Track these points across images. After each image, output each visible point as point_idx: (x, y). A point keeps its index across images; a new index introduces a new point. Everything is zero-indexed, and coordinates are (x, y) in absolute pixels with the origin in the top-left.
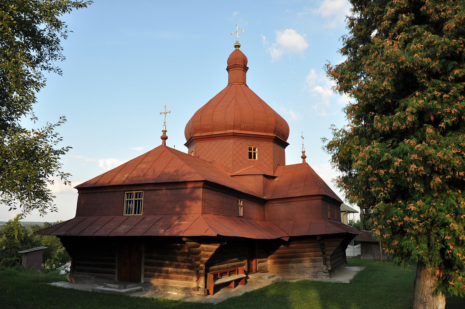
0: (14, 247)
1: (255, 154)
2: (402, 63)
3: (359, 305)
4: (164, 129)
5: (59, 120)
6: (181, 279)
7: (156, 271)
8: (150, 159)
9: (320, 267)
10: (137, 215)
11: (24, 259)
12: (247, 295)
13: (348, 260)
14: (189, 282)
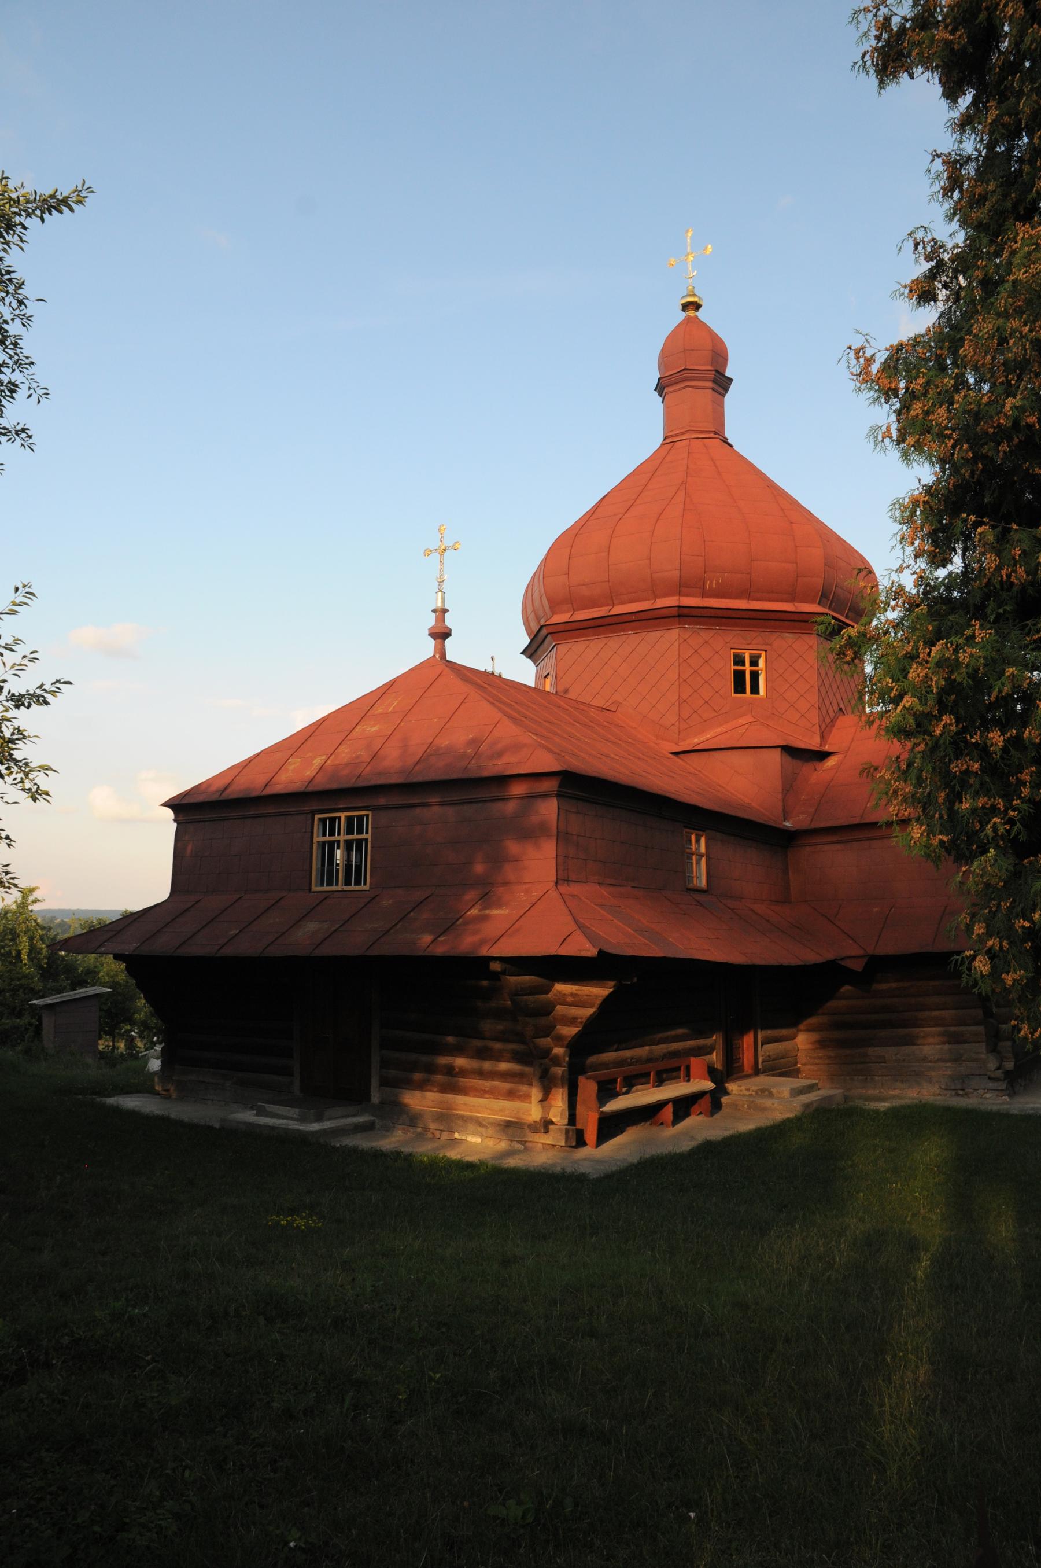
0: (21, 986)
1: (755, 676)
4: (439, 605)
5: (12, 596)
6: (494, 1093)
9: (976, 1060)
10: (353, 887)
11: (48, 1022)
12: (708, 1148)
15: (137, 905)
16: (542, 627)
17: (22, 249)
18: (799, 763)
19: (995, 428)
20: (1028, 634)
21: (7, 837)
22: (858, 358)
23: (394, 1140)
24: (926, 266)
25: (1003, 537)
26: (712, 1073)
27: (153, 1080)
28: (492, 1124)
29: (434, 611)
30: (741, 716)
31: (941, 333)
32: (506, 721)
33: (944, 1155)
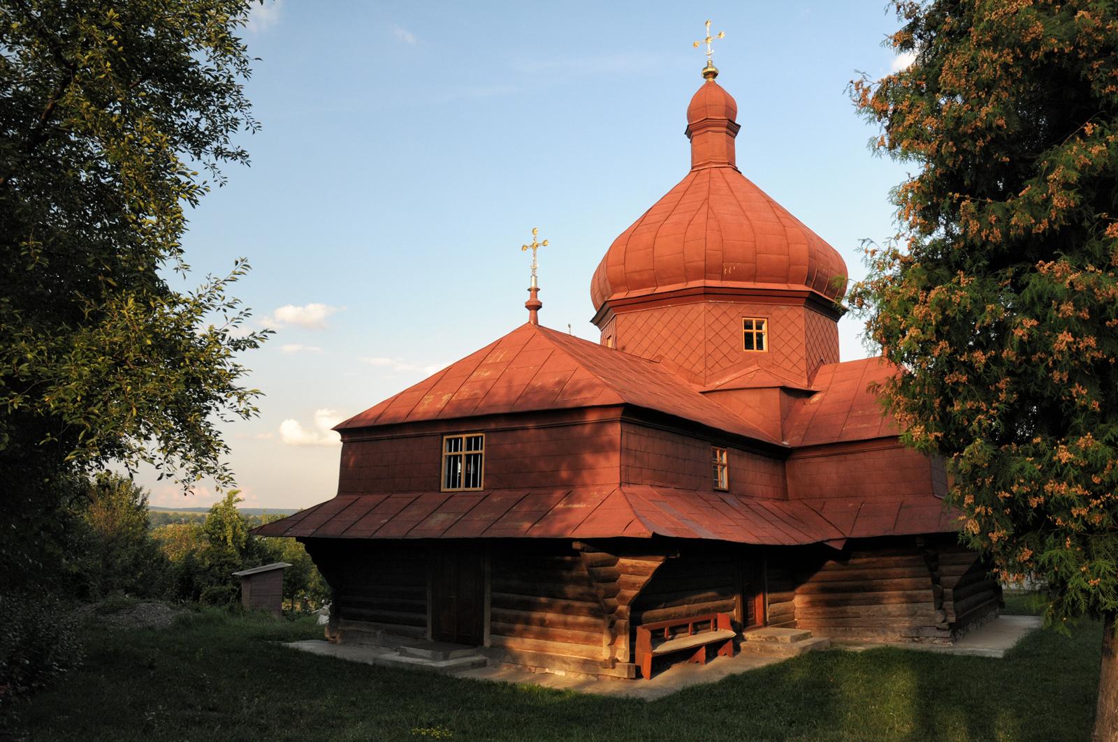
1: (760, 336)
2: (1036, 44)
3: (1020, 717)
4: (533, 285)
6: (574, 639)
7: (516, 620)
8: (499, 356)
9: (926, 616)
10: (471, 489)
11: (246, 590)
12: (733, 680)
13: (1005, 599)
14: (591, 647)
15: (305, 508)
16: (606, 302)
17: (244, 25)
18: (792, 398)
19: (973, 129)
20: (1000, 281)
21: (225, 447)
22: (858, 89)
23: (501, 674)
24: (906, 22)
25: (981, 208)
26: (733, 625)
27: (323, 630)
28: (573, 662)
29: (529, 290)
30: (750, 366)
31: (918, 70)
32: (582, 368)
33: (908, 685)
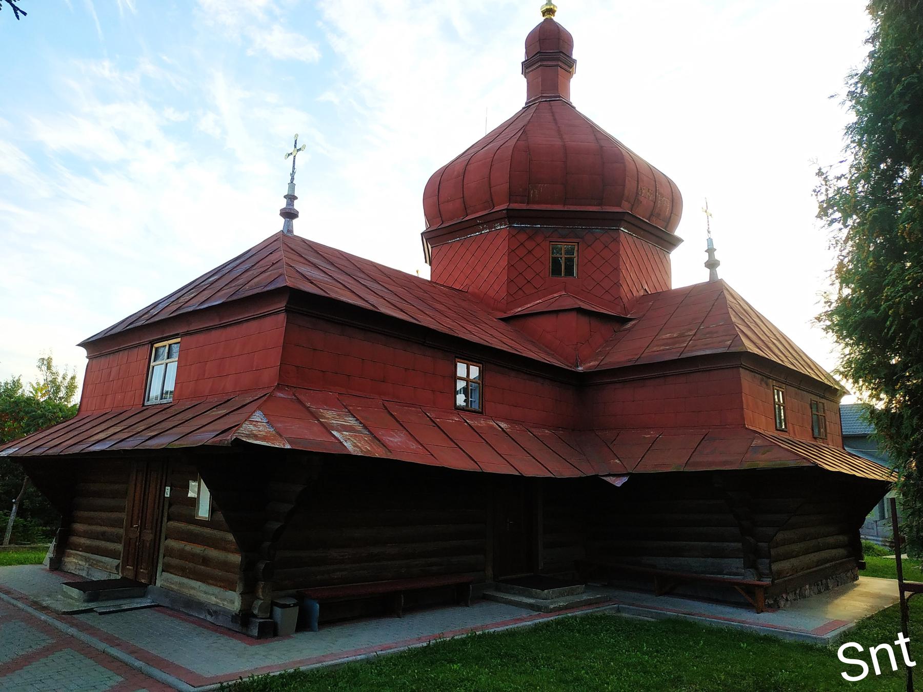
1: (569, 261)
